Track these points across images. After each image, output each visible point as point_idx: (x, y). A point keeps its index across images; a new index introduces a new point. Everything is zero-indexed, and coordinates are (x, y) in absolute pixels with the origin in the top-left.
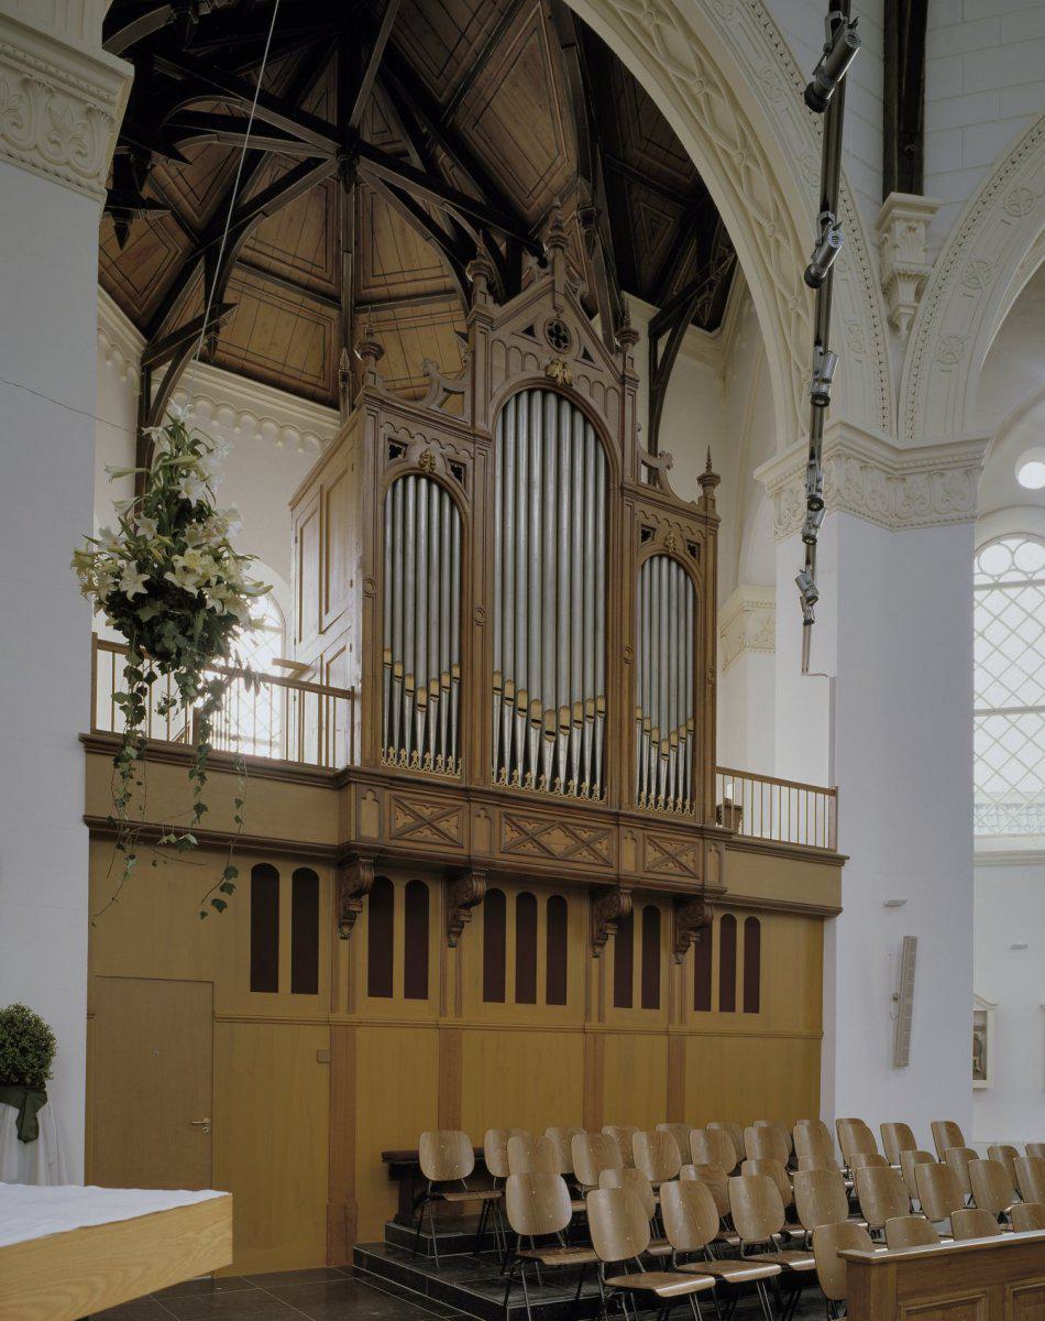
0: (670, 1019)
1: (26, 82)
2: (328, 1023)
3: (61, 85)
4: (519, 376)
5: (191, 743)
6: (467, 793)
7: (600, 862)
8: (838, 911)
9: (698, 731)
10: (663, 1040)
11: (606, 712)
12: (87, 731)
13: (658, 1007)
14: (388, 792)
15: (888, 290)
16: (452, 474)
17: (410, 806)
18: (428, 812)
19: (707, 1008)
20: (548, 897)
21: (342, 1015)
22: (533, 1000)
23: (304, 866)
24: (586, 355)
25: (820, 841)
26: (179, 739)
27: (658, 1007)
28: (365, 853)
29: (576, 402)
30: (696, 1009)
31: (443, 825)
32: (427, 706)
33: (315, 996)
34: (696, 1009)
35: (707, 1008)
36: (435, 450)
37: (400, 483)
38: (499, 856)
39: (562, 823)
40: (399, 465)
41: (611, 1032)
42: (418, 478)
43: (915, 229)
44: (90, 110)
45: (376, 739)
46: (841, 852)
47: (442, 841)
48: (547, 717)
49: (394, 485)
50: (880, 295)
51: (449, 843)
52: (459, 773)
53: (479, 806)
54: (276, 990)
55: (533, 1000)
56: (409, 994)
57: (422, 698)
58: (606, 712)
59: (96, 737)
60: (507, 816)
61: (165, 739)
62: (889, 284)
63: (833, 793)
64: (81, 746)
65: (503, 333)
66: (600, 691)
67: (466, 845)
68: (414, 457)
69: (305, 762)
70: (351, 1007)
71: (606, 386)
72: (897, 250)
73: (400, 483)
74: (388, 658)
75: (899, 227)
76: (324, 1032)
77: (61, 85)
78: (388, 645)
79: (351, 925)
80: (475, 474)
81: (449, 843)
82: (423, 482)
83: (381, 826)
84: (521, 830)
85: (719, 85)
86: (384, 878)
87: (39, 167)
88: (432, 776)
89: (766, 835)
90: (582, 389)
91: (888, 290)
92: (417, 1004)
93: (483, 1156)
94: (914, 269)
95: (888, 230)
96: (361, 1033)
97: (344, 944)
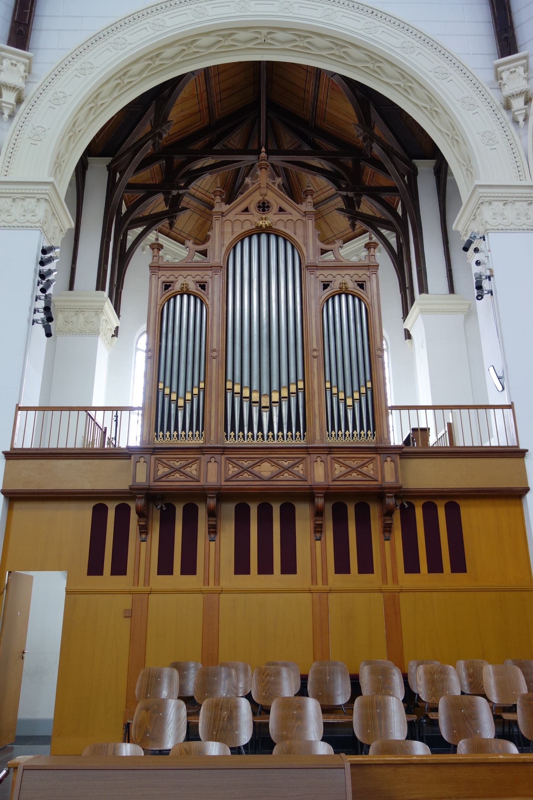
0: (385, 580)
1: (14, 200)
2: (381, 591)
3: (26, 195)
4: (239, 231)
5: (448, 445)
6: (306, 449)
7: (297, 478)
8: (527, 490)
9: (374, 388)
10: (380, 597)
11: (304, 388)
12: (8, 449)
13: (372, 572)
14: (329, 456)
15: (508, 107)
16: (358, 287)
17: (167, 462)
18: (246, 464)
19: (440, 570)
20: (355, 504)
21: (390, 586)
22: (271, 572)
23: (263, 502)
24: (281, 210)
25: (512, 443)
26: (434, 444)
27: (372, 572)
28: (139, 492)
29: (277, 233)
30: (406, 572)
31: (364, 470)
32: (353, 406)
33: (195, 576)
34: (406, 572)
35: (440, 570)
36: (347, 279)
37: (172, 300)
38: (223, 483)
39: (267, 458)
40: (328, 292)
41: (330, 591)
42: (340, 295)
43: (515, 71)
44: (38, 199)
45: (322, 426)
46: (522, 447)
47: (186, 479)
48: (263, 399)
49: (327, 302)
50: (504, 112)
51: (191, 479)
52: (375, 439)
53: (315, 456)
54: (249, 573)
55: (271, 572)
56: (284, 571)
57: (181, 403)
58: (304, 388)
59: (14, 452)
60: (227, 459)
61: (489, 445)
62: (507, 104)
63: (510, 407)
64: (3, 455)
65: (231, 216)
66: (300, 377)
67: (380, 479)
68: (177, 287)
69: (457, 445)
70: (325, 581)
71: (295, 220)
72: (505, 86)
73: (172, 300)
74: (328, 385)
75: (505, 75)
76: (380, 597)
77: (26, 195)
78: (328, 378)
79: (390, 532)
80: (371, 286)
81: (191, 479)
82: (350, 297)
83: (326, 475)
84: (347, 466)
85: (381, 60)
86: (431, 502)
87: (33, 227)
88: (359, 443)
89: (487, 444)
90: (280, 227)
91: (508, 107)
92: (188, 578)
93: (358, 680)
94: (518, 90)
95: (501, 79)
96: (402, 597)
97: (387, 543)
